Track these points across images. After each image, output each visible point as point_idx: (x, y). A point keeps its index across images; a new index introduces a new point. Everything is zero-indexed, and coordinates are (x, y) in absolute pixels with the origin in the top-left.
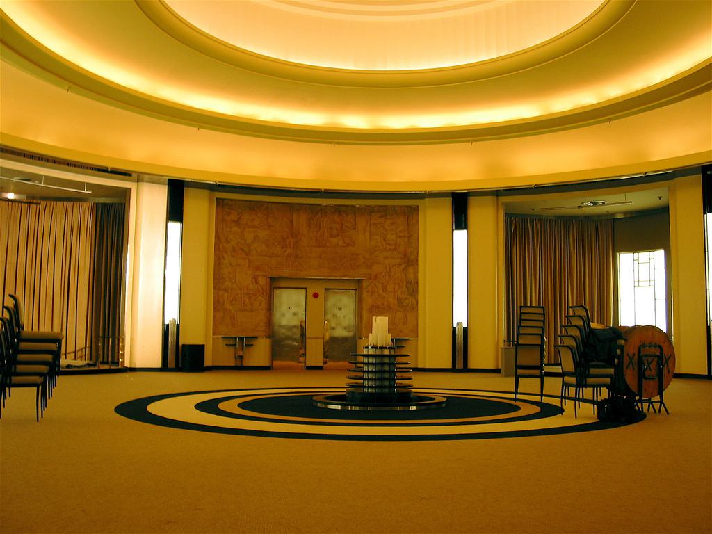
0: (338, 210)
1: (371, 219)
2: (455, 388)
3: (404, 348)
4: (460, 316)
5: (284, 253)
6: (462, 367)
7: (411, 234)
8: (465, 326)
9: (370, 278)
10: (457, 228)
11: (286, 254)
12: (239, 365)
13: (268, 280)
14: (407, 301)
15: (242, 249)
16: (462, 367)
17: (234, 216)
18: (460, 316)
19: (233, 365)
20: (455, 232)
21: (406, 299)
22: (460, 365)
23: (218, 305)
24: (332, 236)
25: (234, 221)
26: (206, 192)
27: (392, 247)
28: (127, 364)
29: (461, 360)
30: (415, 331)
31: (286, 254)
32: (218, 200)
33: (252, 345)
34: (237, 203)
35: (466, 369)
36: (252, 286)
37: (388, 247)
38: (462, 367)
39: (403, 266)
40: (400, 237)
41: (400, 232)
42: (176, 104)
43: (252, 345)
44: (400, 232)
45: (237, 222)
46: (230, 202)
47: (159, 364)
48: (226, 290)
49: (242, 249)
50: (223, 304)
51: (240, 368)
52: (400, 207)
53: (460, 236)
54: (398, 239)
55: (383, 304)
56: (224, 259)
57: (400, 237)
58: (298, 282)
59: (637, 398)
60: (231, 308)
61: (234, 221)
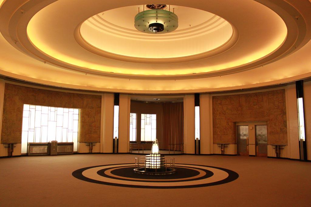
0: (256, 94)
1: (268, 97)
2: (180, 163)
3: (283, 150)
4: (197, 136)
5: (237, 113)
6: (198, 154)
7: (283, 101)
8: (199, 139)
9: (269, 121)
10: (115, 105)
11: (238, 113)
12: (91, 152)
13: (233, 123)
14: (284, 129)
15: (222, 113)
16: (116, 152)
17: (219, 102)
18: (197, 136)
19: (88, 152)
20: (115, 106)
21: (284, 129)
22: (197, 153)
23: (214, 133)
24: (254, 105)
25: (219, 103)
26: (208, 95)
27: (277, 107)
28: (185, 153)
29: (198, 152)
30: (287, 142)
31: (238, 113)
32: (213, 97)
33: (227, 147)
34: (218, 97)
35: (199, 154)
36: (227, 126)
37: (275, 107)
38: (198, 154)
39: (282, 115)
40: (280, 103)
41: (280, 101)
42: (258, 59)
43: (227, 147)
44: (280, 101)
45: (220, 104)
46: (218, 97)
47: (111, 151)
48: (218, 128)
49: (222, 113)
50: (217, 132)
51: (90, 153)
52: (277, 90)
53: (116, 108)
54: (279, 104)
55: (275, 131)
56: (217, 117)
57: (280, 103)
58: (245, 123)
59: (151, 167)
60: (220, 134)
61: (219, 103)
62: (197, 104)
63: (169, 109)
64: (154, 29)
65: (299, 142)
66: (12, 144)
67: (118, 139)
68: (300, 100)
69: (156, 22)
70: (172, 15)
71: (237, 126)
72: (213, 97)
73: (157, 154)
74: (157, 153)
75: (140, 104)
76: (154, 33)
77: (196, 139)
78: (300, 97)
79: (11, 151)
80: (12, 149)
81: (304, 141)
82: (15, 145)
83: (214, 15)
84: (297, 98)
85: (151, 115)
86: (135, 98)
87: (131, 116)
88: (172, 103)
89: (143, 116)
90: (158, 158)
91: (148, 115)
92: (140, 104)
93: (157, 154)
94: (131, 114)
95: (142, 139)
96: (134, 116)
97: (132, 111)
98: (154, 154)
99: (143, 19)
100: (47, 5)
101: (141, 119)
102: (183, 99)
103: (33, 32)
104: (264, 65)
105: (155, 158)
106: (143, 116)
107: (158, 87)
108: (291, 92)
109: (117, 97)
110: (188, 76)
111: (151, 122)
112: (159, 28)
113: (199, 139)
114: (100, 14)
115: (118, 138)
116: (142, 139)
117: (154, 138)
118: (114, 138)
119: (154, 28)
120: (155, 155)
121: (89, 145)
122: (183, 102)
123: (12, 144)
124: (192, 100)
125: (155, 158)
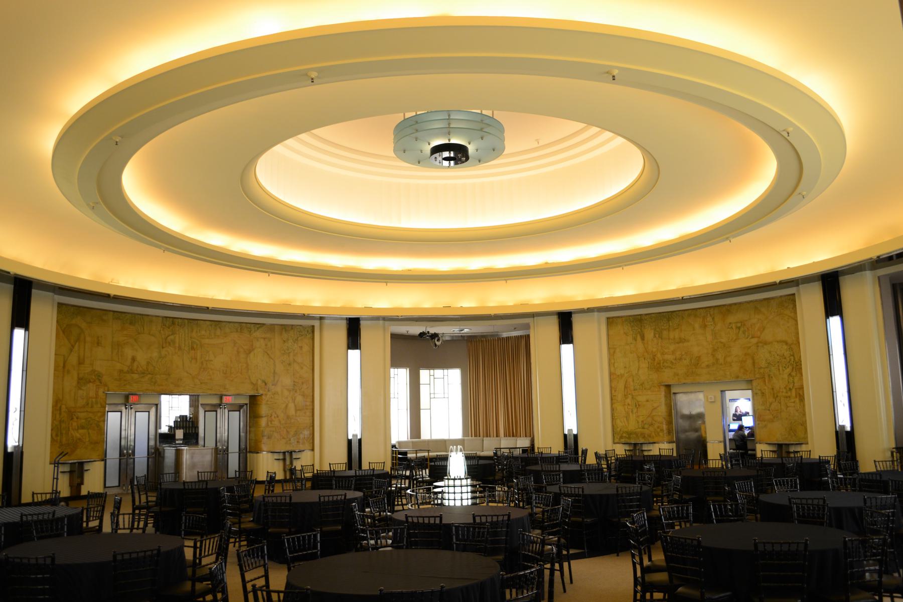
20: (349, 351)
32: (608, 318)
34: (638, 321)
62: (566, 336)
63: (494, 355)
64: (446, 159)
65: (837, 432)
66: (81, 464)
67: (360, 440)
68: (835, 322)
69: (447, 142)
70: (487, 121)
71: (675, 393)
72: (608, 318)
73: (460, 479)
74: (463, 477)
75: (418, 346)
76: (453, 168)
77: (566, 432)
78: (832, 315)
79: (77, 481)
80: (81, 477)
81: (847, 432)
82: (86, 467)
83: (584, 125)
84: (827, 317)
85: (446, 371)
86: (402, 329)
87: (392, 375)
88: (499, 339)
89: (424, 374)
90: (464, 489)
91: (438, 373)
92: (418, 346)
93: (460, 479)
94: (392, 370)
95: (425, 435)
96: (400, 377)
97: (396, 364)
98: (454, 479)
99: (418, 134)
100: (145, 143)
101: (419, 384)
102: (527, 327)
103: (135, 186)
104: (734, 236)
105: (458, 490)
106: (424, 374)
107: (467, 300)
108: (812, 301)
109: (354, 330)
110: (681, 243)
111: (432, 392)
112: (459, 154)
113: (575, 432)
114: (316, 131)
115: (359, 437)
116: (425, 435)
117: (455, 430)
118: (350, 437)
119: (446, 154)
120: (458, 483)
121: (284, 460)
122: (528, 336)
123: (81, 464)
124: (553, 329)
125: (458, 490)
